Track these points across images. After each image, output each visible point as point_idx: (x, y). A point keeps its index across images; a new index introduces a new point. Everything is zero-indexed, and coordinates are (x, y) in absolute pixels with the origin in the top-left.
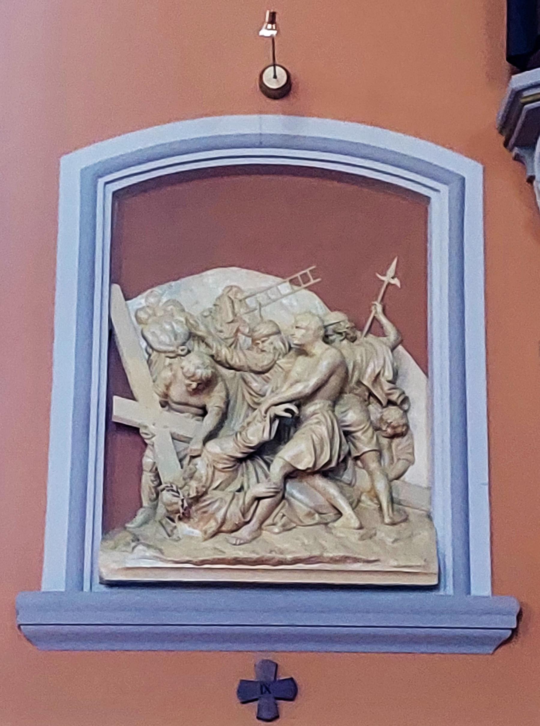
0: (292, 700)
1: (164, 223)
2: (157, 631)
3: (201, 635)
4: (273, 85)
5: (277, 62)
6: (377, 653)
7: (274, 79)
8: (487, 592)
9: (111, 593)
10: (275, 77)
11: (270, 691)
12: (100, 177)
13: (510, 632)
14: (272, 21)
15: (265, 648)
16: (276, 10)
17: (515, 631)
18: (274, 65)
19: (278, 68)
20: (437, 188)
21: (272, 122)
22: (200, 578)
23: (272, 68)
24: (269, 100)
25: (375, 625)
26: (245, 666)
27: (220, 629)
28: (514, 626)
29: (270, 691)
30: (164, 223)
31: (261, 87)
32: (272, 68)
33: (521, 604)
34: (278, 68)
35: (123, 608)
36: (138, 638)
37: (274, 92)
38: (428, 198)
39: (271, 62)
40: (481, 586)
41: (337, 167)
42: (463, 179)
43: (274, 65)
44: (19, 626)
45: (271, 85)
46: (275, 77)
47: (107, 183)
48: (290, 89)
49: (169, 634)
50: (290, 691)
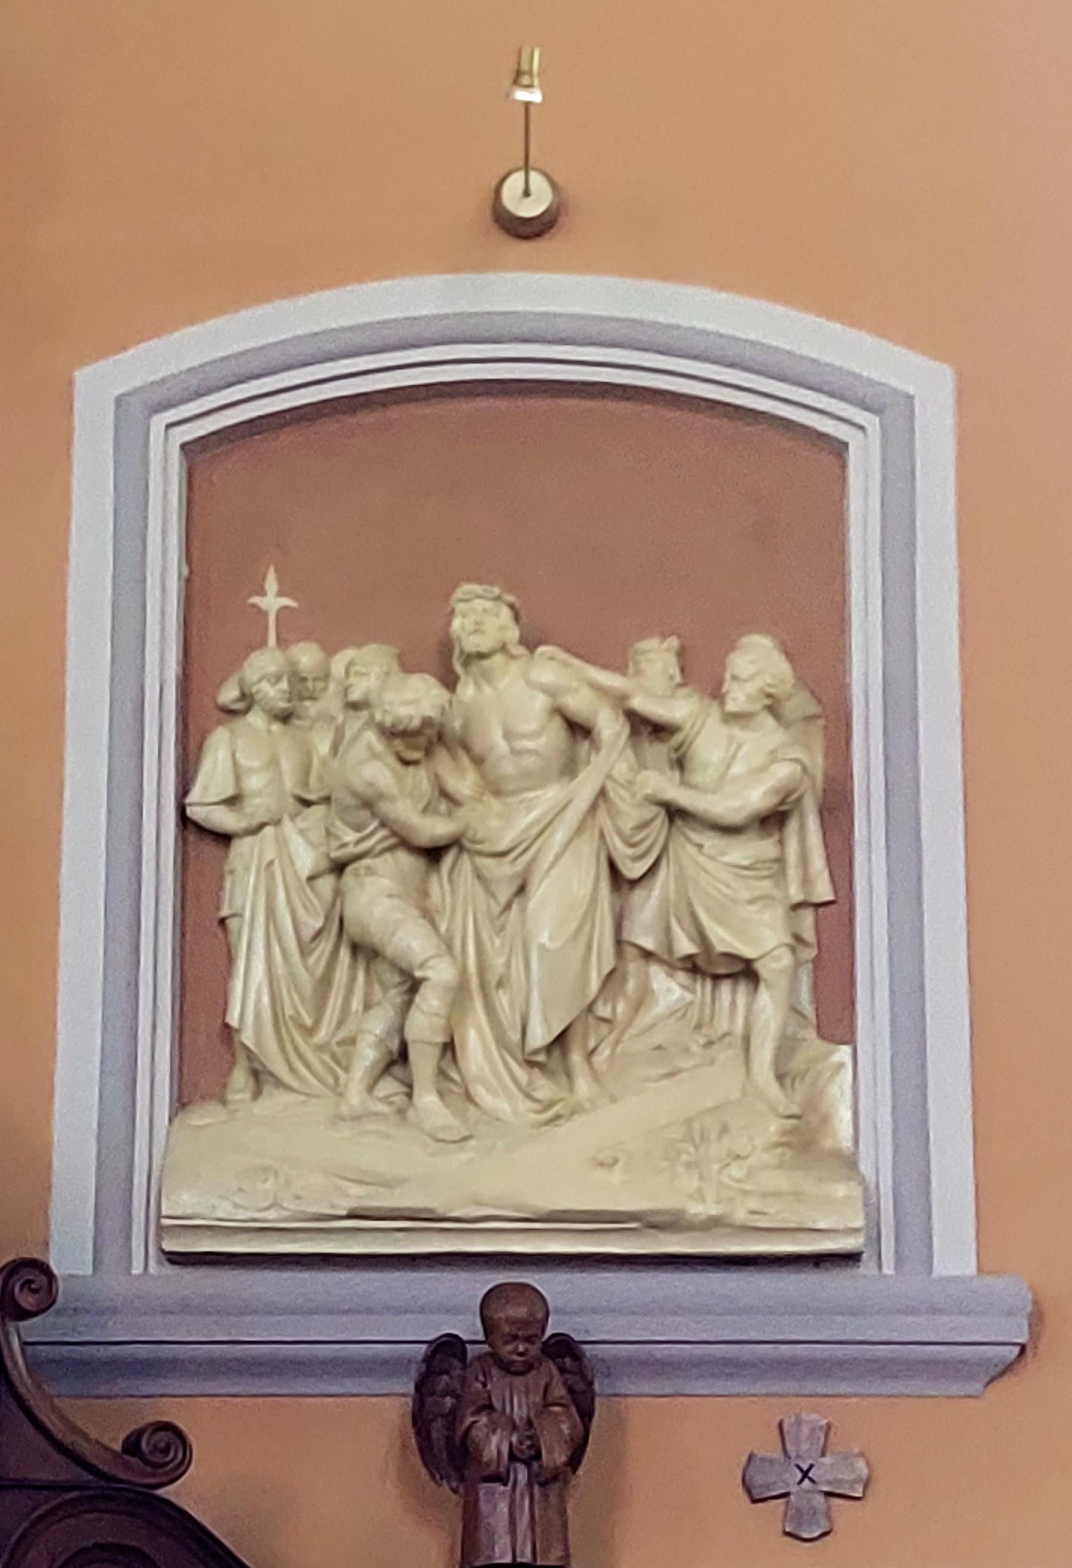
3: (385, 1362)
10: (527, 193)
12: (157, 411)
13: (1016, 1350)
18: (527, 167)
19: (534, 176)
27: (279, 1349)
31: (172, 1262)
34: (534, 176)
39: (521, 163)
40: (955, 1255)
43: (527, 167)
46: (527, 193)
47: (170, 426)
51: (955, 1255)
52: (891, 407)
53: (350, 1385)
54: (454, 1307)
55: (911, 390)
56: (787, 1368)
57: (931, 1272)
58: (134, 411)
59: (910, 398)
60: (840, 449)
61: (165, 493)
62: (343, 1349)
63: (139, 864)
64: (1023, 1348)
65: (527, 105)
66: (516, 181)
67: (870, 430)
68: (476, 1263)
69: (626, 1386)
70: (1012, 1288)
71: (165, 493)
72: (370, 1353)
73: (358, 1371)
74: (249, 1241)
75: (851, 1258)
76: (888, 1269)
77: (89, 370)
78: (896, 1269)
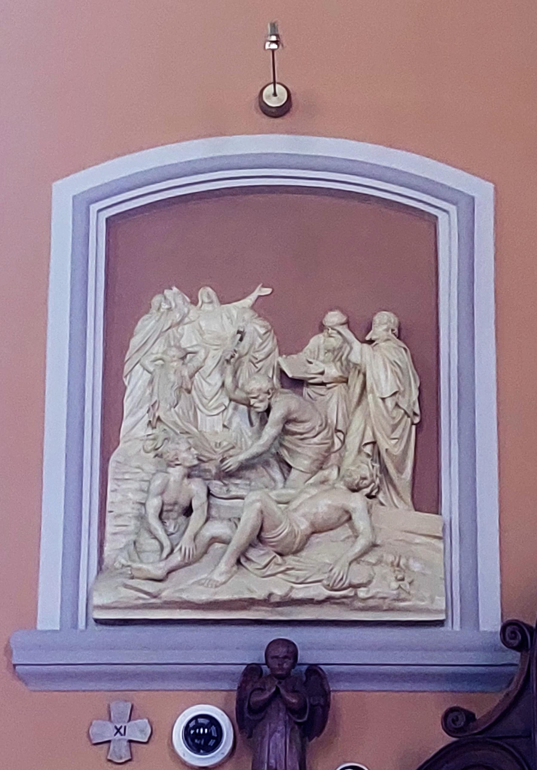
1: (155, 247)
4: (273, 103)
5: (277, 80)
9: (244, 630)
10: (275, 94)
21: (275, 142)
22: (132, 616)
23: (272, 86)
24: (272, 120)
30: (155, 247)
31: (261, 108)
34: (278, 86)
35: (411, 648)
36: (99, 677)
39: (272, 80)
43: (274, 83)
44: (15, 665)
45: (270, 102)
46: (275, 94)
47: (99, 211)
48: (291, 106)
49: (381, 674)
53: (92, 686)
54: (247, 647)
55: (473, 194)
57: (478, 629)
58: (83, 203)
59: (473, 198)
60: (107, 219)
61: (450, 248)
65: (273, 51)
66: (270, 89)
67: (451, 213)
68: (136, 624)
69: (342, 686)
71: (450, 248)
74: (116, 614)
75: (440, 623)
76: (457, 628)
77: (59, 182)
78: (461, 627)
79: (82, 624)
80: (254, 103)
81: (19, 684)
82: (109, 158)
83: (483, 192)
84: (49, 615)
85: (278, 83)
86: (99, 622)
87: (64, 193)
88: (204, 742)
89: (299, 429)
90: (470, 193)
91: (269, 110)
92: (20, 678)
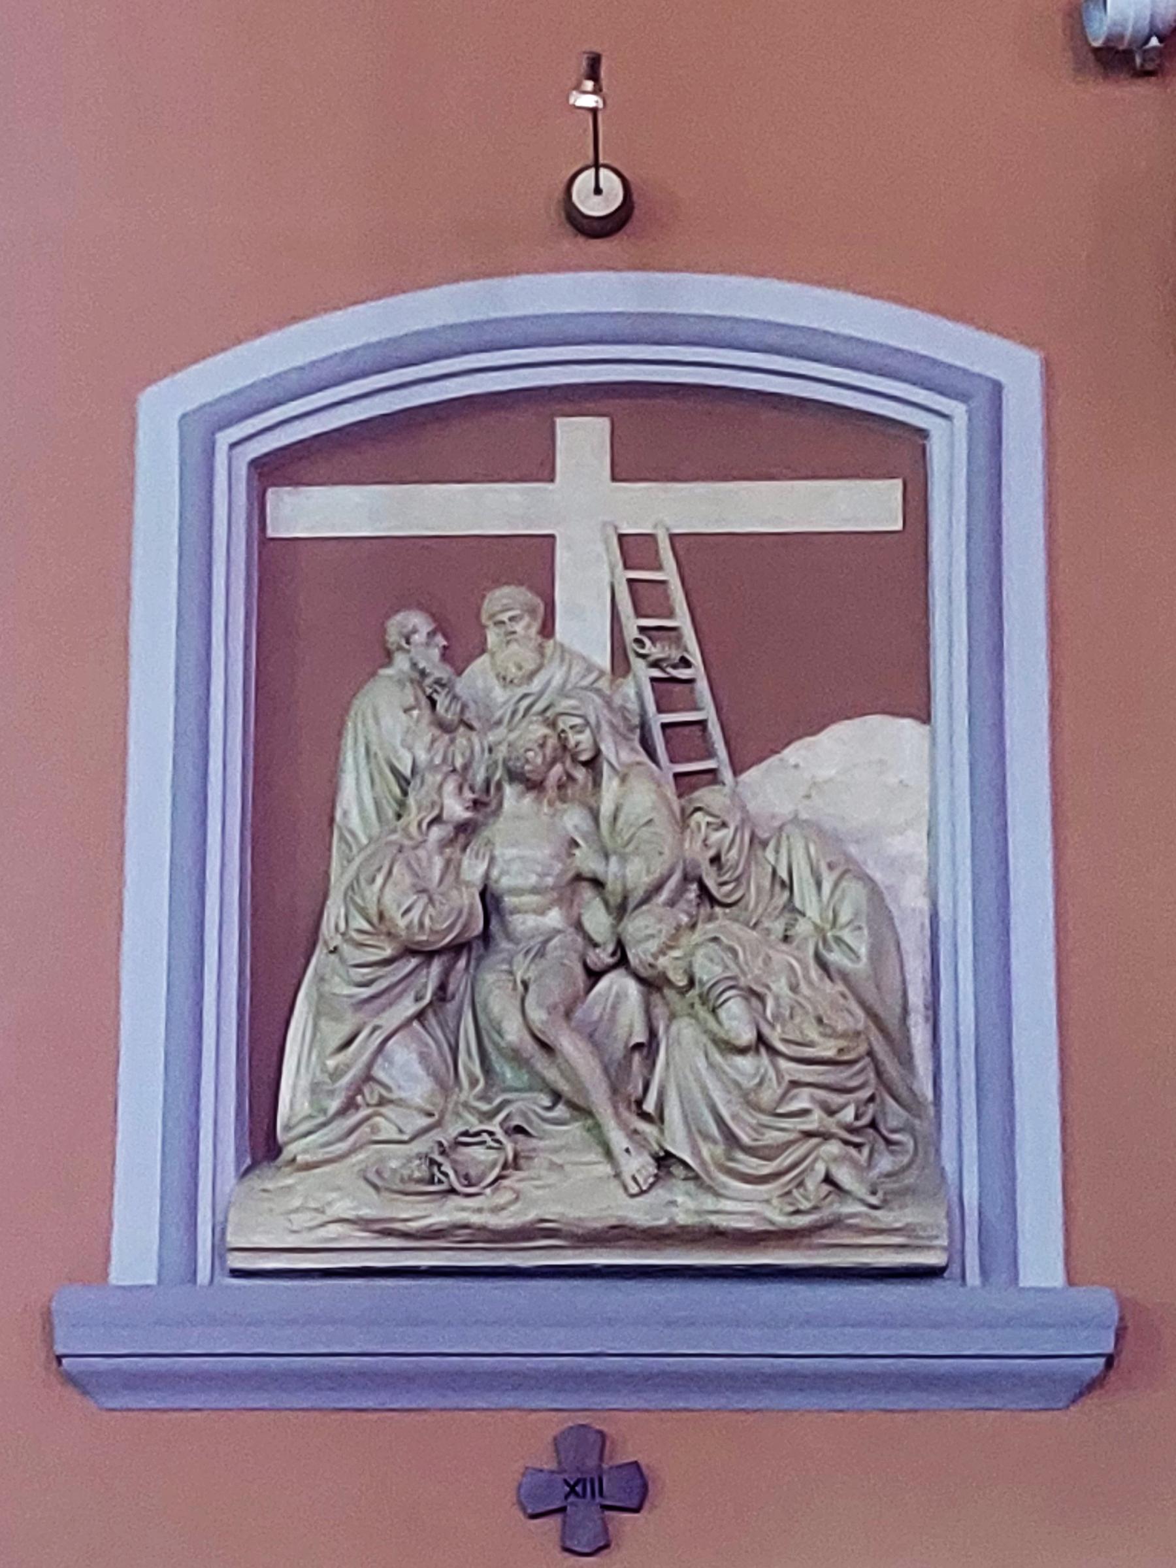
0: (637, 1510)
2: (589, 1369)
3: (361, 1374)
4: (594, 207)
5: (601, 161)
6: (129, 1410)
7: (597, 198)
8: (1058, 1279)
10: (598, 191)
11: (590, 1488)
12: (221, 428)
13: (1101, 1361)
14: (593, 73)
15: (151, 1404)
16: (597, 49)
17: (1110, 1360)
18: (597, 165)
19: (603, 172)
20: (946, 411)
23: (592, 171)
25: (370, 1351)
26: (527, 1439)
27: (683, 1363)
28: (1109, 1348)
29: (590, 1488)
32: (592, 171)
33: (1122, 1303)
34: (603, 172)
37: (595, 224)
38: (923, 433)
40: (1041, 1262)
41: (452, 365)
42: (997, 388)
43: (597, 165)
44: (59, 1358)
46: (598, 191)
47: (233, 446)
48: (632, 208)
50: (637, 1490)
51: (1041, 1262)
52: (204, 427)
56: (769, 1381)
62: (289, 1363)
63: (448, 357)
64: (1110, 1360)
65: (594, 111)
66: (586, 180)
70: (1101, 1301)
72: (254, 1367)
73: (227, 1375)
77: (152, 390)
79: (203, 1275)
80: (555, 214)
81: (72, 1396)
82: (126, 677)
83: (1017, 368)
84: (135, 1252)
85: (606, 166)
86: (237, 1273)
87: (162, 412)
88: (1134, 60)
89: (497, 1210)
90: (991, 373)
91: (585, 221)
92: (70, 1379)
